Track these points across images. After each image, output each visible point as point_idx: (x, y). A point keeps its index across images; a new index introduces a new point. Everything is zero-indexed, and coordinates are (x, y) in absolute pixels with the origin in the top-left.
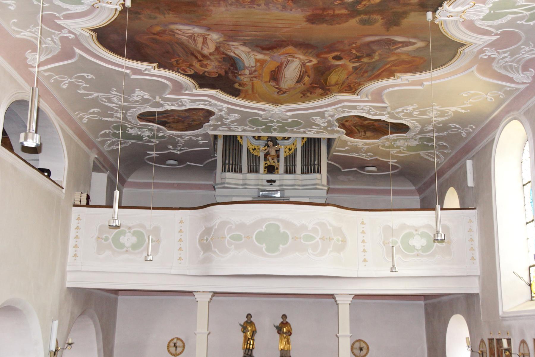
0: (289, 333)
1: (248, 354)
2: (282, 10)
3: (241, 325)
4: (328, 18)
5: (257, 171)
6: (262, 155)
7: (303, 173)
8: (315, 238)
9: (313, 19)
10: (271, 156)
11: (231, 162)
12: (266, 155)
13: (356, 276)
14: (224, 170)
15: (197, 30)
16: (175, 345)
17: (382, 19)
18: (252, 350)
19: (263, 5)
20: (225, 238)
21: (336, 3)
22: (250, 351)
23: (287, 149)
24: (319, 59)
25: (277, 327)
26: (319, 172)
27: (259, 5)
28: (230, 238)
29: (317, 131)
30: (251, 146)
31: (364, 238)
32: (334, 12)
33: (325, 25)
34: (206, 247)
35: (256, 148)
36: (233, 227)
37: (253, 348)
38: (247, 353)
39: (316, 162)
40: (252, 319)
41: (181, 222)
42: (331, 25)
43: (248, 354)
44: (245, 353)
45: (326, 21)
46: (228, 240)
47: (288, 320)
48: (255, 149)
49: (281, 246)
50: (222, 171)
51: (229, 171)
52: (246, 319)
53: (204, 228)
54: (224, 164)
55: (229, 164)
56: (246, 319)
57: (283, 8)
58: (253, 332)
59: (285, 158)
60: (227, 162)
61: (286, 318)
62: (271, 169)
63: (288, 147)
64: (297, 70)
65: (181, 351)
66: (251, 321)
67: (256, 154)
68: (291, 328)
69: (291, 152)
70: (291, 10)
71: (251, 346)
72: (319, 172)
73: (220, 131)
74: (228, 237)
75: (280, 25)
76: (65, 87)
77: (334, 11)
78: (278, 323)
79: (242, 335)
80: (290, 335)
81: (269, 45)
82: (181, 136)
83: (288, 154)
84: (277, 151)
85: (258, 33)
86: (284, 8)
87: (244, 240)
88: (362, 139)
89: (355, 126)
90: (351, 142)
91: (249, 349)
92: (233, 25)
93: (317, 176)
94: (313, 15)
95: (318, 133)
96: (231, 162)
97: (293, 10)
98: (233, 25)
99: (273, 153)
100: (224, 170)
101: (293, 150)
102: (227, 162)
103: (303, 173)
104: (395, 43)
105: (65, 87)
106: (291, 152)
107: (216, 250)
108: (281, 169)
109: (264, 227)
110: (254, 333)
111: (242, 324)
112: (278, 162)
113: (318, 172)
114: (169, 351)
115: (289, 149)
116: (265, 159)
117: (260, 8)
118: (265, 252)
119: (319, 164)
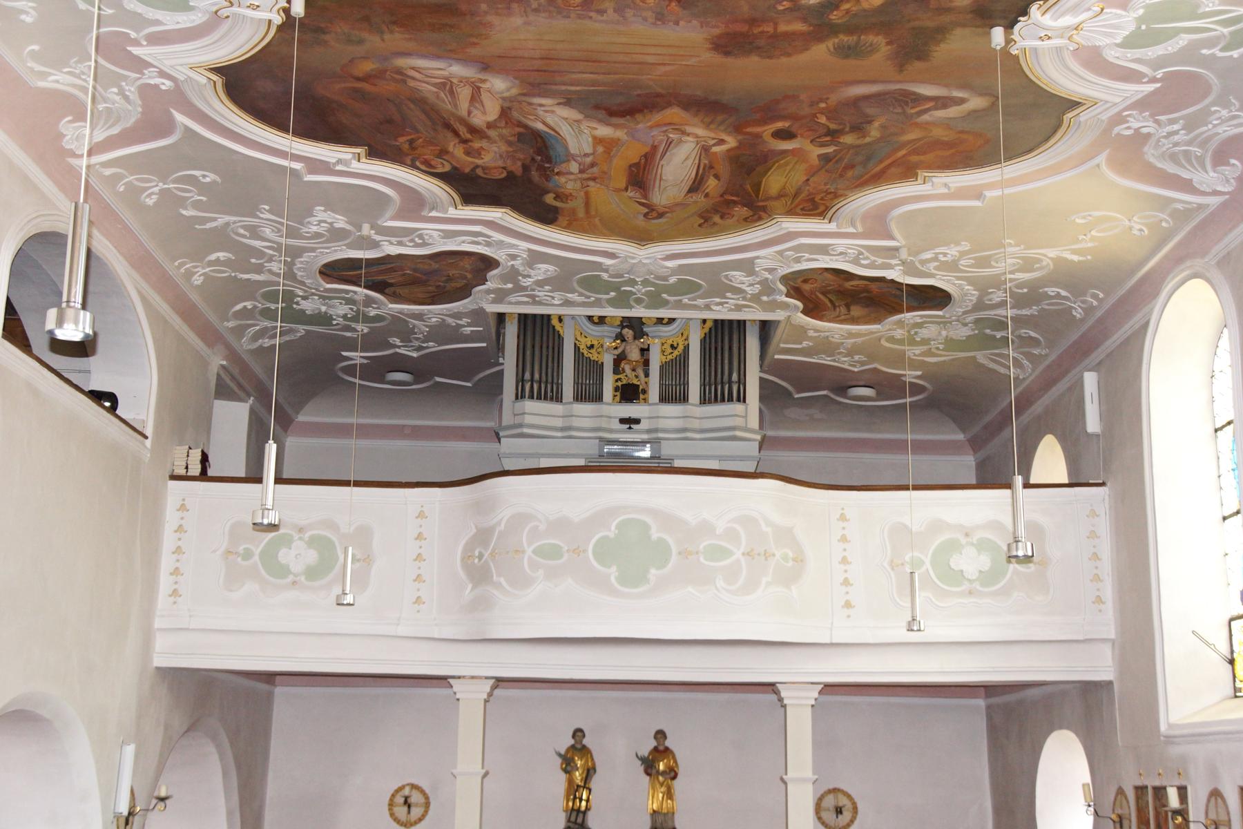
0: (672, 774)
1: (575, 823)
2: (654, 24)
3: (560, 755)
4: (761, 42)
5: (598, 398)
6: (608, 360)
7: (704, 401)
8: (731, 553)
9: (728, 45)
10: (630, 362)
11: (537, 376)
12: (618, 361)
13: (828, 641)
14: (520, 396)
15: (457, 70)
16: (406, 802)
17: (888, 44)
18: (585, 813)
19: (610, 11)
20: (523, 552)
21: (781, 8)
22: (581, 815)
23: (667, 347)
24: (740, 137)
25: (644, 760)
26: (742, 399)
27: (601, 12)
28: (534, 552)
29: (736, 305)
30: (583, 340)
31: (845, 554)
32: (775, 29)
33: (755, 59)
34: (478, 573)
35: (595, 343)
36: (542, 527)
37: (587, 809)
38: (573, 819)
39: (735, 377)
40: (585, 742)
41: (421, 515)
42: (770, 57)
43: (575, 823)
44: (569, 821)
45: (758, 48)
46: (530, 558)
47: (668, 743)
48: (592, 346)
49: (653, 571)
50: (517, 398)
51: (531, 397)
52: (572, 742)
53: (474, 531)
54: (520, 380)
55: (532, 380)
56: (572, 742)
57: (657, 19)
58: (588, 771)
59: (661, 367)
60: (527, 376)
61: (665, 737)
62: (629, 393)
63: (670, 342)
64: (690, 162)
65: (420, 815)
66: (584, 747)
67: (594, 357)
68: (675, 762)
69: (676, 353)
70: (677, 23)
71: (584, 803)
72: (742, 399)
73: (510, 303)
74: (529, 551)
75: (650, 59)
76: (150, 202)
77: (776, 25)
78: (645, 751)
79: (563, 777)
80: (674, 778)
81: (624, 103)
82: (419, 316)
83: (670, 357)
84: (644, 351)
85: (600, 77)
86: (660, 18)
87: (566, 557)
88: (841, 322)
89: (824, 294)
90: (816, 331)
91: (578, 811)
92: (542, 59)
93: (738, 408)
94: (728, 34)
95: (739, 308)
96: (537, 376)
97: (682, 23)
98: (542, 59)
99: (634, 355)
100: (520, 396)
101: (681, 348)
102: (527, 376)
103: (704, 401)
104: (918, 99)
105: (150, 202)
106: (676, 353)
107: (502, 580)
108: (654, 393)
109: (613, 528)
110: (590, 772)
111: (563, 752)
112: (647, 375)
113: (739, 400)
114: (392, 815)
115: (672, 346)
116: (617, 370)
117: (605, 18)
118: (616, 584)
119: (742, 382)
